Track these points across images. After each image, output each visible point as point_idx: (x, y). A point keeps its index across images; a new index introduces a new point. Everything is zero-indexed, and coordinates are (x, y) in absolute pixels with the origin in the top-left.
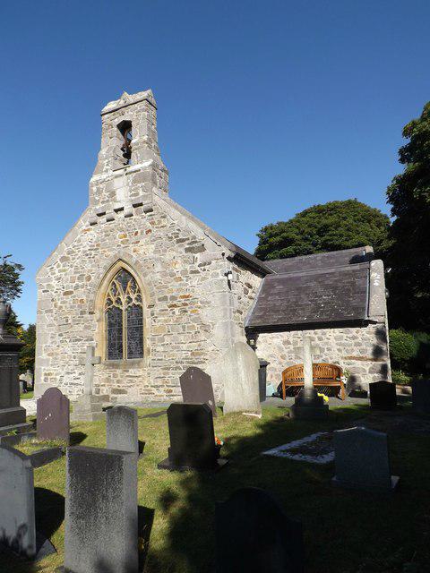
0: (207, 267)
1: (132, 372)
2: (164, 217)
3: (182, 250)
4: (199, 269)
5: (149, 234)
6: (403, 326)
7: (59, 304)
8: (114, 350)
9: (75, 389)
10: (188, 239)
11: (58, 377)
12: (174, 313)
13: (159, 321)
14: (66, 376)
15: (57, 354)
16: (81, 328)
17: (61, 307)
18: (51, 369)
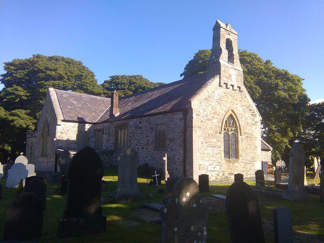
1: (236, 164)
3: (250, 114)
6: (254, 187)
7: (205, 125)
8: (227, 154)
9: (214, 173)
11: (206, 167)
14: (210, 166)
15: (204, 154)
16: (215, 140)
18: (201, 162)
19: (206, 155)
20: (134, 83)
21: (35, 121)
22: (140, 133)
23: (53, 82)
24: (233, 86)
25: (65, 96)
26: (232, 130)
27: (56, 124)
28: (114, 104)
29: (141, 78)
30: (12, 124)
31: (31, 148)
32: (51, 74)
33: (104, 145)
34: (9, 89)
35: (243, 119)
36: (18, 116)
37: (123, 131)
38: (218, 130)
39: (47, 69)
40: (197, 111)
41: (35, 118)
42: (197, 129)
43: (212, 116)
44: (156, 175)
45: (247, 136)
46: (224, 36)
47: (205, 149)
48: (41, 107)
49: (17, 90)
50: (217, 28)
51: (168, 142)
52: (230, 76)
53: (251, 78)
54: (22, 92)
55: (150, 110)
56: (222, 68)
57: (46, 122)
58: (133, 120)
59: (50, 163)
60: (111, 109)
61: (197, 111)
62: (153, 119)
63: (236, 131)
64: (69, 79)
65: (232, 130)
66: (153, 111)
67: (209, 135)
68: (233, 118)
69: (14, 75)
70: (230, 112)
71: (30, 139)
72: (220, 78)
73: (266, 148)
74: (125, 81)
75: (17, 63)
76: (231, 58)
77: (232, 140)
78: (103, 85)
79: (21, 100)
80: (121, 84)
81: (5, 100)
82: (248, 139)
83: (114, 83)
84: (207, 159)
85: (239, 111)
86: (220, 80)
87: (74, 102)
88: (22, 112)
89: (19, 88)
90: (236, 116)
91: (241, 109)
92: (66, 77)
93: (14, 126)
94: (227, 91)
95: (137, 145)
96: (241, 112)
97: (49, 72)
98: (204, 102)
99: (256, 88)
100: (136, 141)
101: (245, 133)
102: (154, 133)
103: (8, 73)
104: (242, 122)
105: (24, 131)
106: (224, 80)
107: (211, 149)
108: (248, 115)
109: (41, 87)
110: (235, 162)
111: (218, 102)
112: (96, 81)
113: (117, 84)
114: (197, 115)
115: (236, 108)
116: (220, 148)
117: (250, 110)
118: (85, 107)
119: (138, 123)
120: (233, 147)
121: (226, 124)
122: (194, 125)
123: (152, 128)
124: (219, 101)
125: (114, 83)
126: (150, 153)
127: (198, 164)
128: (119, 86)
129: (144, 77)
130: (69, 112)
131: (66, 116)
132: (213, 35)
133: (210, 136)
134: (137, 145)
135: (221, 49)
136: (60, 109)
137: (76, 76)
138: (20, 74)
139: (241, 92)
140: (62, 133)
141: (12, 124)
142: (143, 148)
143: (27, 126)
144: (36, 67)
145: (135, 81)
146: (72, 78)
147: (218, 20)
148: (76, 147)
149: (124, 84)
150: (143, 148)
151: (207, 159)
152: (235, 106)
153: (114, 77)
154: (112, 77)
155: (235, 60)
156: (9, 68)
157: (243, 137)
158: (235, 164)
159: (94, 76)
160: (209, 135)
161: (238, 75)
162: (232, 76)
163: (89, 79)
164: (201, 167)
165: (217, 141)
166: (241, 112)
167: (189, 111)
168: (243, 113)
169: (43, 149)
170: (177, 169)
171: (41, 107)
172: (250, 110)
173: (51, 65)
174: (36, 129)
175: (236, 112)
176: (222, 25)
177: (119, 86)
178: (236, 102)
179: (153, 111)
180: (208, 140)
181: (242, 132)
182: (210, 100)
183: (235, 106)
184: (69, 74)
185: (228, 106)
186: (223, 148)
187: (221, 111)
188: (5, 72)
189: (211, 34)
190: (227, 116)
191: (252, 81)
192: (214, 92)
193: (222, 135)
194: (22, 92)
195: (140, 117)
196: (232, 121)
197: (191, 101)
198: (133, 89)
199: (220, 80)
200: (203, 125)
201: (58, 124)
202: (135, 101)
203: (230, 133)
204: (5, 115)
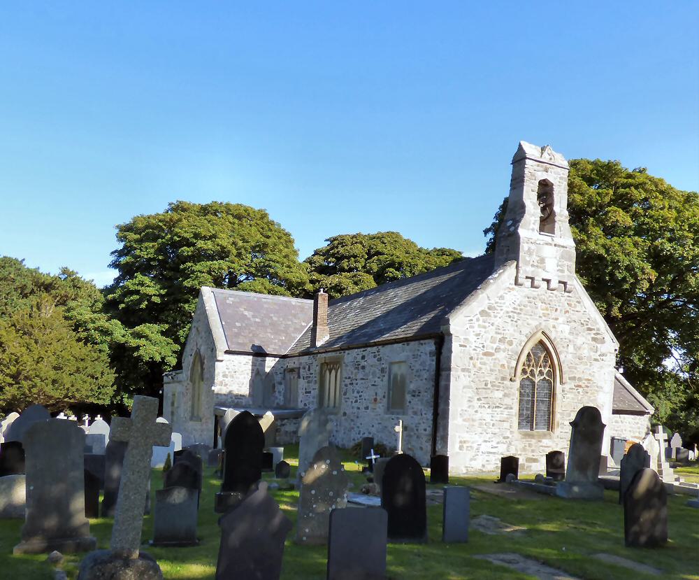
0: (604, 358)
2: (579, 302)
3: (589, 337)
4: (599, 358)
5: (567, 315)
7: (478, 365)
10: (594, 329)
11: (475, 446)
12: (579, 392)
13: (568, 398)
14: (484, 444)
15: (473, 420)
16: (499, 394)
17: (481, 368)
18: (466, 437)
19: (476, 424)
20: (378, 253)
21: (177, 347)
22: (362, 379)
23: (209, 263)
24: (548, 281)
25: (230, 300)
26: (541, 373)
27: (214, 359)
28: (319, 317)
29: (394, 238)
30: (135, 354)
31: (173, 404)
32: (205, 247)
33: (299, 400)
34: (129, 283)
35: (571, 349)
36: (146, 337)
37: (333, 372)
38: (508, 373)
39: (197, 236)
40: (462, 337)
41: (177, 341)
42: (461, 374)
44: (374, 457)
45: (577, 383)
46: (533, 175)
47: (476, 412)
48: (187, 317)
49: (142, 284)
50: (519, 159)
51: (408, 397)
52: (542, 261)
53: (636, 244)
54: (151, 288)
55: (381, 333)
56: (524, 247)
57: (198, 354)
58: (350, 351)
59: (205, 433)
60: (314, 330)
61: (462, 337)
62: (385, 350)
63: (552, 374)
64: (239, 255)
65: (541, 373)
66: (387, 337)
67: (486, 385)
68: (546, 349)
69: (138, 252)
70: (540, 336)
71: (171, 385)
72: (517, 267)
73: (637, 407)
74: (358, 249)
75: (140, 225)
76: (547, 221)
77: (541, 394)
78: (310, 261)
79: (152, 305)
80: (348, 258)
81: (123, 305)
82: (580, 390)
83: (333, 256)
84: (480, 430)
85: (560, 331)
86: (517, 272)
87: (246, 313)
88: (151, 329)
89: (147, 280)
90: (552, 343)
91: (567, 328)
92: (235, 252)
93: (139, 358)
94: (534, 292)
95: (356, 401)
96: (566, 334)
97: (200, 244)
99: (642, 270)
100: (355, 394)
102: (386, 379)
103: (125, 247)
104: (566, 357)
105: (156, 368)
106: (526, 269)
107: (489, 411)
108: (584, 339)
109: (187, 277)
110: (544, 436)
111: (510, 317)
112: (295, 253)
113: (340, 258)
114: (461, 346)
115: (554, 327)
116: (511, 408)
117: (589, 329)
118: (268, 322)
119: (359, 357)
120: (544, 407)
122: (453, 365)
123: (383, 370)
124: (517, 311)
125: (333, 256)
126: (378, 417)
127: (458, 440)
128: (345, 264)
129: (405, 236)
130: (237, 335)
131: (232, 342)
132: (512, 175)
133: (489, 386)
134: (356, 401)
135: (523, 207)
136: (221, 330)
137: (253, 248)
138: (148, 251)
139: (569, 292)
140: (225, 376)
141: (135, 354)
142: (367, 408)
143: (163, 359)
144: (176, 234)
145: (380, 247)
146: (246, 250)
147: (522, 143)
148: (251, 403)
149: (355, 257)
150: (367, 408)
151: (480, 430)
152: (552, 322)
153: (335, 239)
154: (332, 240)
155: (557, 225)
156: (125, 237)
157: (566, 386)
158: (543, 440)
159: (291, 242)
160: (486, 385)
161: (562, 257)
162: (546, 260)
163: (280, 251)
164: (465, 445)
165: (505, 395)
166: (566, 334)
167: (446, 337)
168: (571, 337)
169: (193, 406)
170: (421, 448)
171: (187, 317)
172: (589, 329)
173: (205, 228)
174: (179, 366)
175: (552, 336)
176: (531, 150)
177: (345, 264)
178: (554, 315)
179: (387, 337)
180: (483, 394)
181: (565, 376)
182: (492, 314)
183: (552, 322)
184: (240, 243)
185: (534, 323)
186: (516, 407)
187: (517, 335)
188: (120, 246)
189: (509, 170)
191: (636, 251)
192: (502, 297)
193: (517, 384)
194: (151, 288)
195: (364, 347)
196: (543, 352)
197: (448, 320)
198: (375, 268)
199: (517, 272)
200: (474, 366)
201: (219, 358)
202: (363, 309)
203: (537, 379)
204: (123, 336)
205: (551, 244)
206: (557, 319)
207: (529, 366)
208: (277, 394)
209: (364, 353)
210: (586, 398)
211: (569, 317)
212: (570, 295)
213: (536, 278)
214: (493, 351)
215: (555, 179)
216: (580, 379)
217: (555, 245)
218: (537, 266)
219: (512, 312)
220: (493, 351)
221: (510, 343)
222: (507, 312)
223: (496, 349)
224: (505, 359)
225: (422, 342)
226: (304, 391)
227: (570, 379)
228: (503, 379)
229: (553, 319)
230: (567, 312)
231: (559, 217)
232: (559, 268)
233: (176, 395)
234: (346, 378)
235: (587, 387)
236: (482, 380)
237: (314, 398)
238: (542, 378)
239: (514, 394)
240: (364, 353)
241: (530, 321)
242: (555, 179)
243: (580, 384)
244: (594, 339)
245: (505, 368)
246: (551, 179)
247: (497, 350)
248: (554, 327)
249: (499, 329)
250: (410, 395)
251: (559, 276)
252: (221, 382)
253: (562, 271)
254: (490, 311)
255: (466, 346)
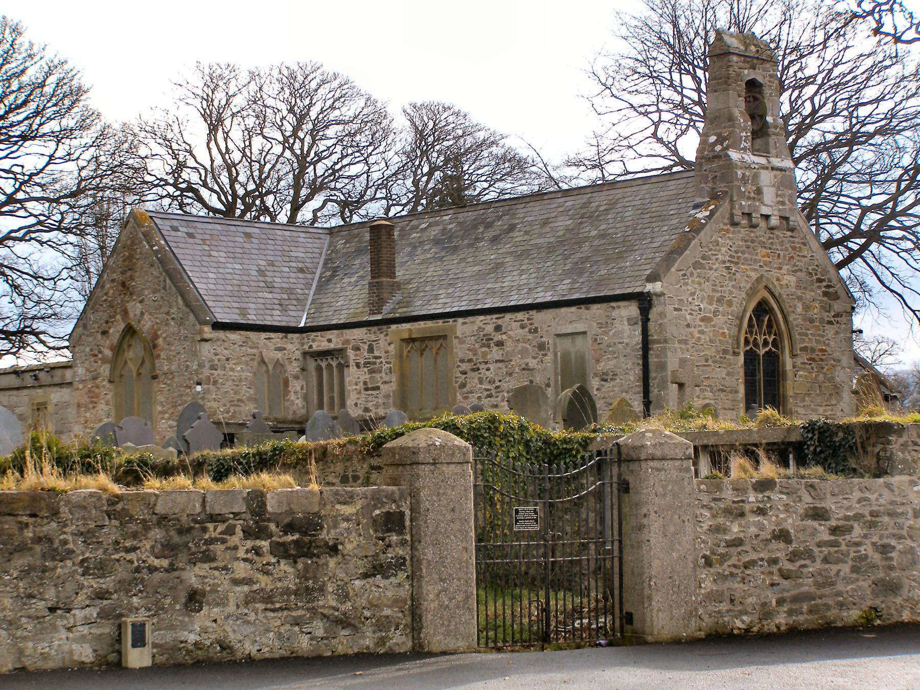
0: (839, 319)
2: (804, 244)
4: (832, 319)
17: (699, 338)
26: (766, 343)
43: (712, 308)
52: (759, 191)
67: (707, 361)
86: (648, 156)
91: (792, 279)
98: (692, 275)
101: (804, 349)
115: (778, 279)
117: (819, 281)
119: (490, 328)
121: (750, 325)
152: (775, 274)
157: (799, 361)
160: (707, 361)
165: (728, 374)
172: (819, 281)
175: (777, 291)
185: (754, 275)
190: (753, 305)
193: (741, 359)
205: (767, 168)
206: (780, 268)
207: (751, 333)
208: (292, 397)
209: (500, 322)
210: (821, 375)
211: (795, 265)
212: (794, 234)
213: (754, 215)
214: (711, 315)
215: (764, 77)
216: (813, 350)
217: (773, 169)
218: (754, 198)
219: (729, 261)
220: (711, 315)
221: (730, 303)
222: (724, 262)
223: (714, 312)
224: (724, 324)
225: (613, 304)
226: (361, 386)
227: (801, 349)
228: (725, 352)
229: (776, 268)
230: (792, 257)
231: (773, 130)
232: (779, 199)
233: (51, 408)
234: (462, 361)
235: (822, 360)
236: (702, 354)
237: (387, 396)
238: (767, 349)
239: (738, 373)
240: (500, 322)
241: (749, 273)
242: (764, 77)
243: (814, 356)
244: (825, 294)
245: (725, 337)
246: (760, 79)
247: (716, 313)
248: (778, 279)
249: (716, 285)
250: (597, 379)
251: (779, 210)
252: (208, 378)
253: (783, 203)
254: (704, 262)
255: (681, 310)
